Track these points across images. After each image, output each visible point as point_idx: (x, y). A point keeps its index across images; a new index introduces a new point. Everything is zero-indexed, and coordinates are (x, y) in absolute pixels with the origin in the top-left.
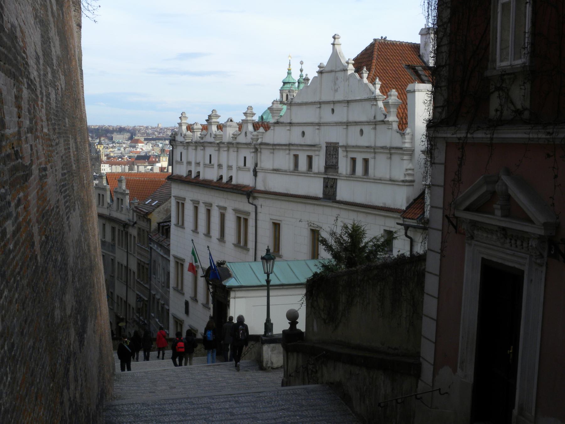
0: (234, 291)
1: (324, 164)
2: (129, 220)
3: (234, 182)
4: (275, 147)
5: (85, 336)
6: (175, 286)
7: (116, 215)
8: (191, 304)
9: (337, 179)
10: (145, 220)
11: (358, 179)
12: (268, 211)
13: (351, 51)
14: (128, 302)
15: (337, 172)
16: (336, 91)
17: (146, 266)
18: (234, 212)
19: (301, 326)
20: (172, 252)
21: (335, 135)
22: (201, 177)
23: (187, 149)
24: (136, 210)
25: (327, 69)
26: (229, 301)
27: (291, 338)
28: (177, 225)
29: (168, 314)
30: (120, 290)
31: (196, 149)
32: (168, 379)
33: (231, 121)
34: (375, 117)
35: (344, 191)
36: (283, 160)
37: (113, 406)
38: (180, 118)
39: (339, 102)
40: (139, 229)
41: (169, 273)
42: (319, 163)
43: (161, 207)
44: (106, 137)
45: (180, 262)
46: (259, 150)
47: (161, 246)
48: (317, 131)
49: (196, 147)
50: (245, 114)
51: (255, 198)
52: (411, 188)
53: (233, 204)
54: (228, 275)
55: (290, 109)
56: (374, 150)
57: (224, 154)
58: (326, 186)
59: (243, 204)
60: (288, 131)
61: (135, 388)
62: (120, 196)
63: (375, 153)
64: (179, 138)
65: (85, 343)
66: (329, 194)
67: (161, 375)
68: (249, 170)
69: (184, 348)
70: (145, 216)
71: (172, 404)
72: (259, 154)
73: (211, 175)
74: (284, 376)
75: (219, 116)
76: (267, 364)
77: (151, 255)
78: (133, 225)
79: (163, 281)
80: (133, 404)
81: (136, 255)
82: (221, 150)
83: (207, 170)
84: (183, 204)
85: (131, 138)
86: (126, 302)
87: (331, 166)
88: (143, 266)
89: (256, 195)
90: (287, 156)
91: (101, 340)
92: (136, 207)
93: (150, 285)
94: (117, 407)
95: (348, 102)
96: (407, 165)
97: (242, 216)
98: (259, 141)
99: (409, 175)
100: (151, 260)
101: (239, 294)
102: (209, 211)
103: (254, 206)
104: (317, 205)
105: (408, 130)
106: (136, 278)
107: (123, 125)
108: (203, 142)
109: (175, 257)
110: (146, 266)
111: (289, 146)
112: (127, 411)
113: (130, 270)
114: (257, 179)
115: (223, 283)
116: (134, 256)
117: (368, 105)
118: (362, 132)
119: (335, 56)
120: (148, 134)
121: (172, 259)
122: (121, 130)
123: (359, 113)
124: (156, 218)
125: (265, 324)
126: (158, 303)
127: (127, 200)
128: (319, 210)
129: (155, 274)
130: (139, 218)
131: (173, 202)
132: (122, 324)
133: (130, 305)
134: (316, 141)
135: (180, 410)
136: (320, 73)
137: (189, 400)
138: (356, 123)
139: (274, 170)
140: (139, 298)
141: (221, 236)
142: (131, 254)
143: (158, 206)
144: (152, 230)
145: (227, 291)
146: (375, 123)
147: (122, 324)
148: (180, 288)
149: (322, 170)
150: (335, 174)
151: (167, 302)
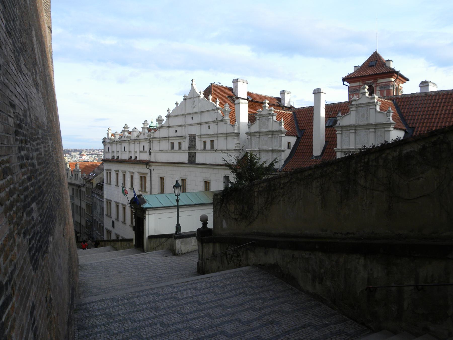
3: (138, 159)
4: (160, 139)
5: (51, 239)
7: (74, 182)
8: (115, 222)
11: (208, 152)
12: (157, 172)
13: (200, 88)
14: (82, 223)
16: (194, 108)
18: (138, 174)
19: (210, 225)
20: (105, 197)
21: (194, 130)
22: (120, 159)
24: (85, 179)
25: (188, 97)
26: (145, 217)
27: (203, 235)
28: (107, 183)
29: (103, 228)
30: (78, 219)
31: (116, 145)
32: (116, 266)
34: (217, 119)
35: (200, 158)
36: (166, 145)
37: (84, 304)
39: (196, 113)
41: (103, 208)
42: (185, 145)
44: (69, 154)
47: (98, 195)
49: (117, 144)
50: (143, 124)
51: (150, 166)
52: (239, 153)
53: (137, 170)
54: (144, 202)
56: (217, 135)
57: (132, 146)
58: (189, 157)
59: (143, 169)
61: (94, 275)
62: (76, 173)
63: (217, 137)
64: (107, 141)
65: (51, 247)
66: (192, 160)
67: (111, 263)
69: (118, 243)
70: (90, 181)
71: (139, 296)
73: (125, 157)
74: (199, 259)
76: (178, 251)
80: (103, 300)
82: (131, 143)
84: (110, 173)
85: (80, 154)
86: (80, 224)
87: (192, 146)
89: (151, 164)
91: (69, 243)
92: (85, 177)
93: (93, 214)
94: (88, 306)
95: (201, 112)
96: (236, 141)
97: (143, 176)
98: (152, 137)
99: (238, 146)
100: (93, 203)
101: (151, 212)
104: (185, 167)
105: (236, 123)
107: (76, 149)
109: (106, 199)
112: (99, 310)
115: (142, 206)
117: (212, 113)
118: (209, 127)
119: (193, 90)
120: (87, 152)
121: (104, 200)
122: (75, 151)
123: (207, 118)
124: (95, 182)
125: (176, 227)
126: (97, 223)
127: (80, 174)
128: (186, 169)
131: (105, 173)
132: (78, 235)
134: (183, 134)
135: (149, 303)
136: (185, 99)
137: (154, 291)
138: (206, 123)
139: (160, 151)
143: (96, 176)
145: (144, 211)
146: (217, 122)
147: (78, 235)
148: (109, 215)
149: (187, 148)
151: (102, 222)
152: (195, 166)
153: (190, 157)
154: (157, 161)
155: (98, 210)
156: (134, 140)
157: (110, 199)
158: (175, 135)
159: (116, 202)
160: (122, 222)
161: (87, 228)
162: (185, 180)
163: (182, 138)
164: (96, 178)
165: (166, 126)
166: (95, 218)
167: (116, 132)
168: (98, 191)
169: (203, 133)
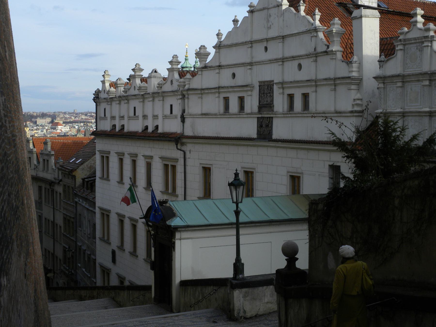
0: (180, 231)
1: (258, 104)
2: (55, 179)
6: (101, 236)
8: (118, 252)
9: (272, 117)
15: (273, 111)
17: (72, 220)
23: (111, 104)
26: (174, 243)
28: (102, 178)
33: (156, 72)
35: (281, 129)
36: (213, 104)
38: (103, 76)
40: (65, 186)
41: (95, 225)
42: (252, 103)
46: (186, 96)
47: (86, 199)
49: (120, 101)
50: (171, 62)
51: (183, 144)
55: (219, 52)
58: (260, 126)
60: (218, 75)
64: (102, 96)
66: (265, 133)
68: (176, 117)
72: (186, 100)
73: (136, 126)
75: (143, 70)
78: (59, 183)
79: (89, 232)
82: (146, 101)
84: (108, 158)
88: (69, 221)
90: (217, 99)
98: (187, 87)
101: (185, 235)
102: (134, 162)
103: (182, 152)
108: (127, 96)
109: (101, 209)
110: (72, 220)
113: (57, 225)
114: (186, 124)
116: (61, 212)
128: (253, 151)
129: (80, 227)
130: (64, 176)
133: (57, 257)
134: (248, 81)
139: (202, 114)
141: (148, 185)
142: (57, 210)
143: (82, 163)
144: (77, 186)
145: (172, 231)
148: (106, 238)
149: (256, 109)
150: (270, 113)
160: (131, 253)
163: (245, 89)
165: (214, 64)
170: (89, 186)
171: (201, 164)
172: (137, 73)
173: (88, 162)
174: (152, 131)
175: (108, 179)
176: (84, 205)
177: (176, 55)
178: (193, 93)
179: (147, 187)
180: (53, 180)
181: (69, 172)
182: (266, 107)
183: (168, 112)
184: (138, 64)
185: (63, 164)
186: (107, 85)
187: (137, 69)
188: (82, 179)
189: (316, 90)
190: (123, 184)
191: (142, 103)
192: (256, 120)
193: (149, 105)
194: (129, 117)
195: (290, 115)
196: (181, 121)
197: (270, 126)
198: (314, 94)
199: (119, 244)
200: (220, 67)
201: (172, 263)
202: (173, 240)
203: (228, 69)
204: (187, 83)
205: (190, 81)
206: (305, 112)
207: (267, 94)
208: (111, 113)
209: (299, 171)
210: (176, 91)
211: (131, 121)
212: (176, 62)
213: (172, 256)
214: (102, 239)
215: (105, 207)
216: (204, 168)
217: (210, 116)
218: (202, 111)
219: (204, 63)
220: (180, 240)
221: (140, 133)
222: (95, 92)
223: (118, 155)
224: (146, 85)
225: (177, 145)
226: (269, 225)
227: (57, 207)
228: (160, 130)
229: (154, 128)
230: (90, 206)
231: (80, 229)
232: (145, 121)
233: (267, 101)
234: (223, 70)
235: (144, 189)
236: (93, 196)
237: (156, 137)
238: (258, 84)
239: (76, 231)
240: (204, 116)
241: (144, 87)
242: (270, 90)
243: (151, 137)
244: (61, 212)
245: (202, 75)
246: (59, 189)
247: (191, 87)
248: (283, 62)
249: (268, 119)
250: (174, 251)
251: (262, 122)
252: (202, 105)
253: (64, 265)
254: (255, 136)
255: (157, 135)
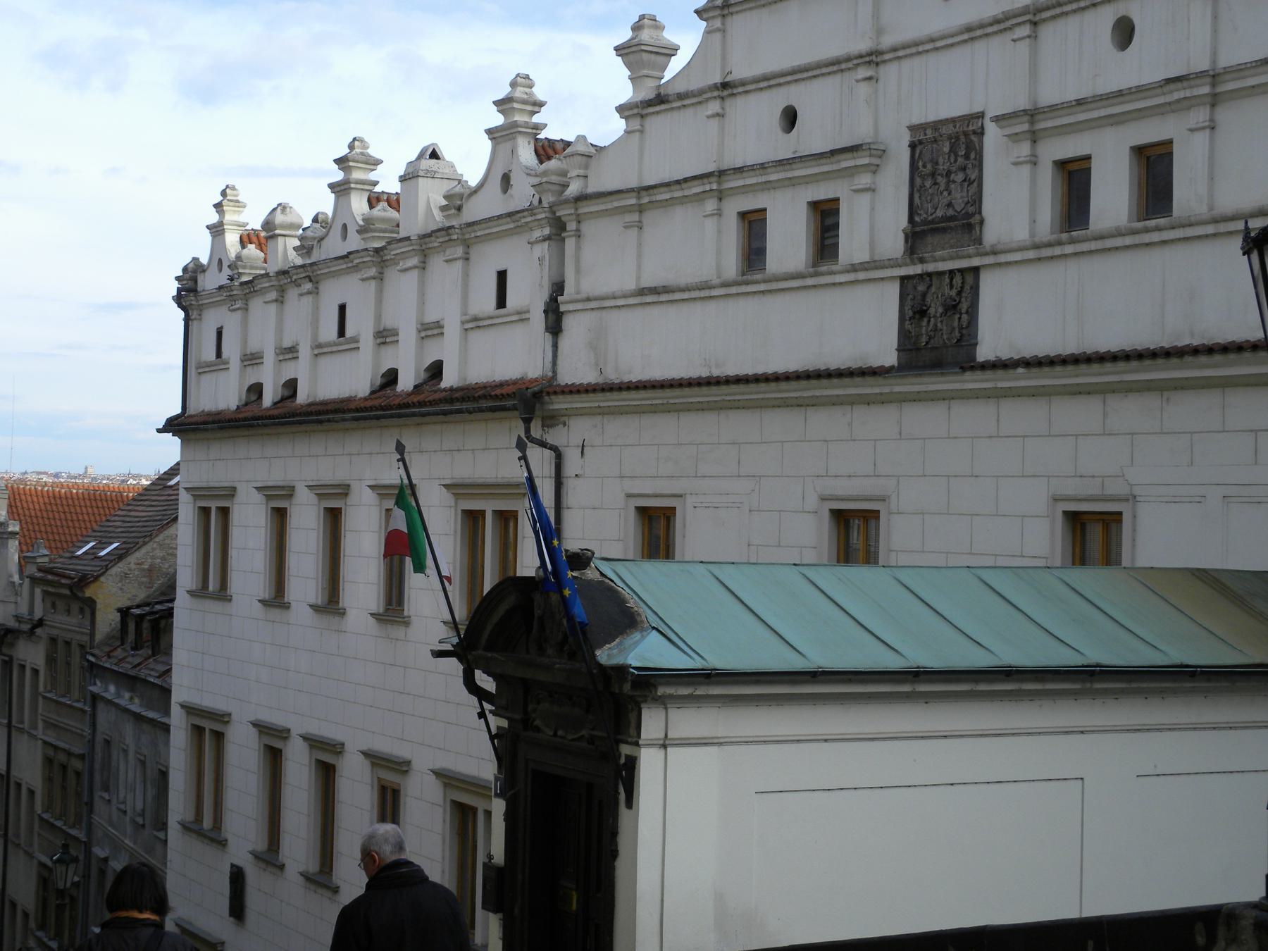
0: (663, 702)
1: (904, 222)
2: (18, 618)
6: (190, 816)
8: (255, 878)
9: (976, 270)
10: (75, 607)
15: (979, 241)
17: (77, 764)
23: (246, 309)
26: (632, 764)
28: (200, 592)
33: (434, 155)
35: (1010, 316)
36: (696, 244)
38: (218, 206)
40: (53, 640)
41: (164, 775)
42: (877, 220)
43: (132, 559)
45: (208, 725)
46: (572, 226)
47: (131, 681)
48: (864, 88)
49: (282, 291)
50: (503, 105)
51: (551, 420)
55: (723, 31)
58: (914, 309)
60: (714, 123)
64: (210, 282)
66: (938, 336)
68: (522, 316)
72: (570, 244)
73: (348, 378)
75: (378, 162)
77: (94, 725)
78: (31, 632)
79: (139, 806)
81: (40, 732)
82: (391, 274)
83: (329, 365)
84: (225, 512)
88: (64, 768)
90: (710, 224)
98: (574, 188)
100: (92, 742)
101: (687, 721)
102: (334, 517)
103: (547, 452)
106: (38, 809)
108: (312, 264)
109: (190, 710)
110: (77, 764)
111: (716, 182)
113: (19, 785)
114: (565, 342)
115: (606, 655)
116: (34, 737)
121: (177, 719)
124: (113, 595)
128: (878, 423)
129: (106, 788)
130: (54, 605)
133: (14, 905)
134: (861, 131)
139: (642, 292)
140: (45, 880)
141: (389, 601)
142: (21, 730)
143: (119, 556)
144: (99, 636)
145: (619, 702)
148: (207, 823)
149: (893, 242)
150: (971, 250)
152: (972, 382)
153: (921, 313)
154: (613, 376)
155: (130, 791)
156: (424, 237)
157: (219, 705)
158: (784, 146)
159: (262, 728)
160: (308, 878)
161: (42, 926)
162: (870, 517)
163: (847, 162)
164: (116, 570)
165: (695, 84)
166: (99, 852)
167: (283, 207)
168: (127, 660)
169: (1049, 95)
170: (146, 633)
171: (629, 496)
172: (356, 175)
173: (143, 550)
174: (416, 387)
175: (223, 594)
176: (123, 702)
177: (527, 77)
178: (603, 207)
179: (387, 610)
180: (12, 624)
181: (70, 587)
182: (944, 230)
183: (485, 301)
184: (361, 140)
185: (51, 561)
186: (232, 239)
187: (353, 160)
188: (119, 610)
189: (1212, 120)
190: (286, 606)
191: (373, 283)
192: (894, 290)
193: (403, 287)
194: (320, 346)
195: (1069, 249)
196: (547, 329)
197: (964, 306)
198: (1202, 139)
199: (262, 846)
200: (726, 88)
201: (613, 868)
202: (625, 750)
203: (765, 95)
204: (573, 173)
205: (586, 167)
206: (1153, 223)
207: (949, 173)
208: (245, 341)
209: (1122, 490)
210: (530, 210)
211: (324, 361)
212: (524, 102)
213: (614, 834)
214: (192, 828)
215: (208, 702)
216: (643, 512)
217: (677, 296)
218: (638, 278)
219: (652, 83)
220: (664, 746)
221: (366, 399)
222: (185, 269)
223: (269, 498)
224: (392, 213)
225: (527, 421)
226: (1075, 695)
227: (22, 722)
228: (450, 379)
229: (423, 376)
230: (150, 707)
231: (106, 796)
232: (387, 351)
233: (950, 205)
234: (740, 101)
235: (372, 620)
236: (162, 668)
237: (432, 403)
238: (906, 138)
239: (90, 805)
240: (649, 299)
241: (383, 220)
242: (967, 157)
243: (414, 405)
244: (34, 737)
245: (641, 132)
246: (32, 654)
247: (591, 189)
248: (1035, 24)
249: (957, 280)
250: (630, 803)
251: (924, 295)
252: (639, 256)
253: (39, 934)
254: (890, 358)
255: (437, 396)
